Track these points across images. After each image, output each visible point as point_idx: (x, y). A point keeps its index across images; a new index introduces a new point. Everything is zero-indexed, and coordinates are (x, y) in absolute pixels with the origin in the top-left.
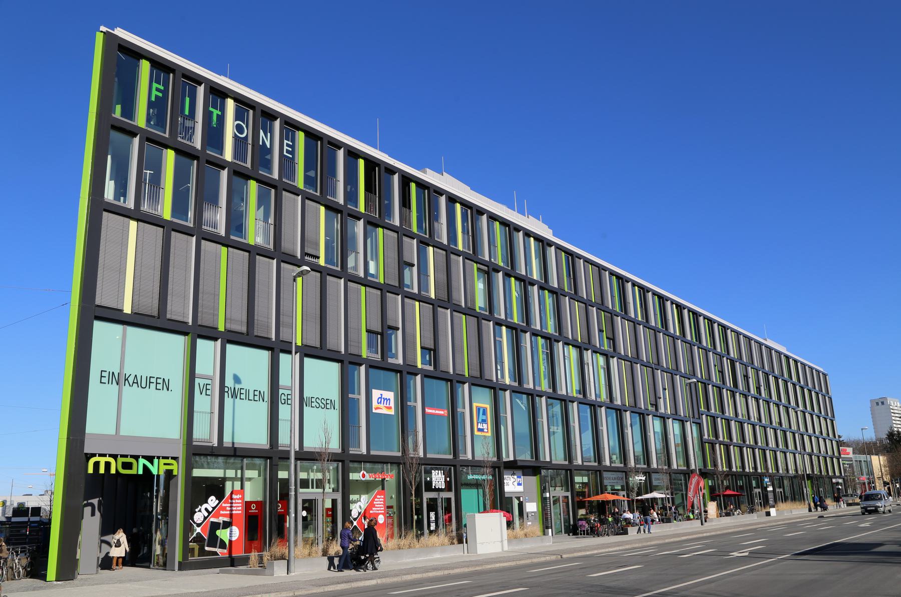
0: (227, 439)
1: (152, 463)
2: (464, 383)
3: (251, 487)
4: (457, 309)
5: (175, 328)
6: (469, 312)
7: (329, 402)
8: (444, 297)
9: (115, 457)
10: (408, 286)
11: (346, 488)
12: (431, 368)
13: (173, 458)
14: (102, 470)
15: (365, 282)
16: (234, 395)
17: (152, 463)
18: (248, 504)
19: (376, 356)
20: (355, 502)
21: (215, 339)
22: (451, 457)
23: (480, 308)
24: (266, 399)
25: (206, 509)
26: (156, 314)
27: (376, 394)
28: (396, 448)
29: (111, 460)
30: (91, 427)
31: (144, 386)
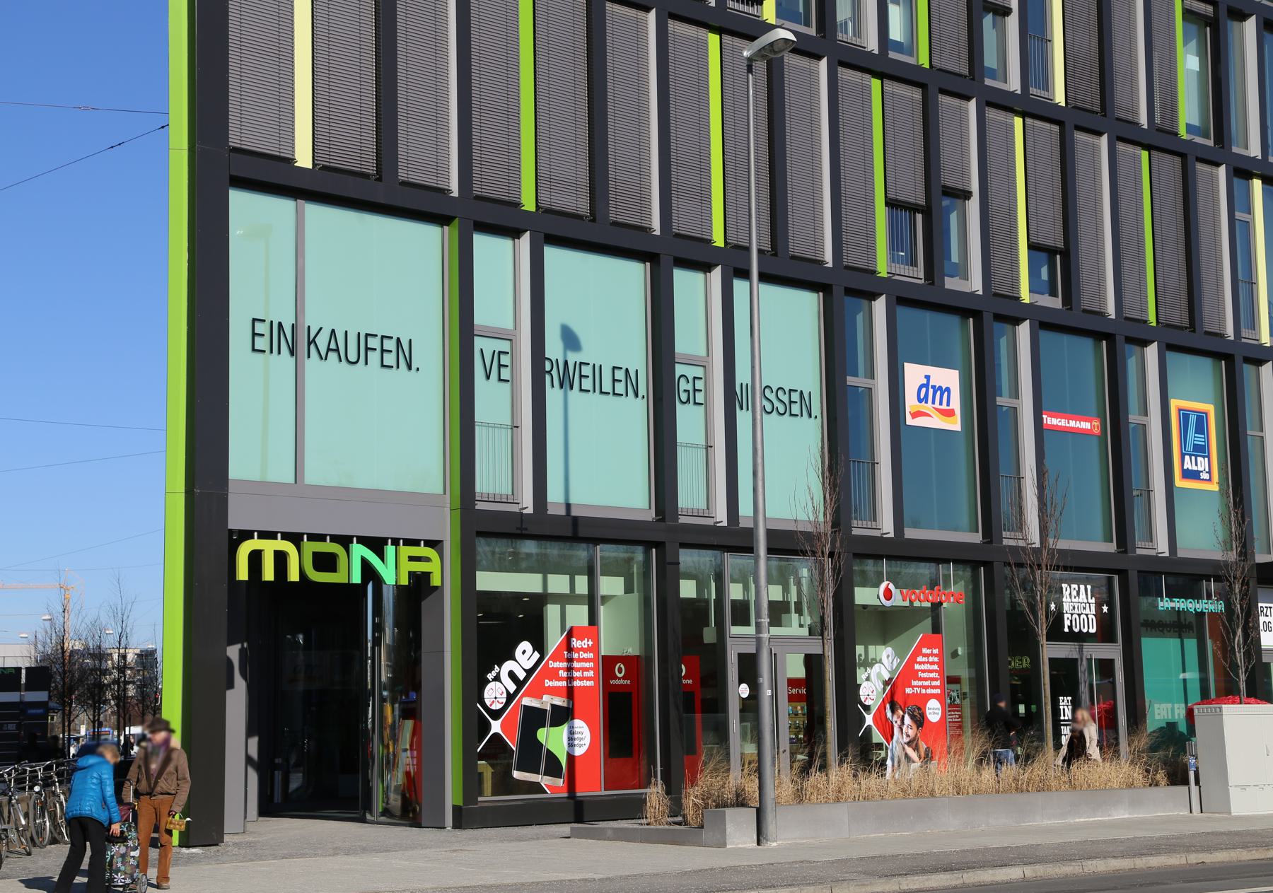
0: (555, 495)
1: (381, 555)
2: (1145, 343)
3: (599, 621)
4: (1126, 134)
5: (418, 205)
6: (1160, 140)
7: (795, 397)
8: (1091, 99)
9: (295, 538)
10: (993, 74)
11: (847, 628)
12: (1056, 303)
13: (431, 544)
14: (269, 574)
15: (883, 67)
16: (566, 382)
17: (381, 555)
18: (608, 663)
19: (909, 270)
20: (868, 664)
21: (514, 234)
22: (977, 538)
23: (1189, 127)
24: (642, 390)
25: (512, 675)
26: (370, 168)
27: (914, 374)
28: (965, 520)
29: (288, 547)
30: (245, 462)
31: (353, 358)
